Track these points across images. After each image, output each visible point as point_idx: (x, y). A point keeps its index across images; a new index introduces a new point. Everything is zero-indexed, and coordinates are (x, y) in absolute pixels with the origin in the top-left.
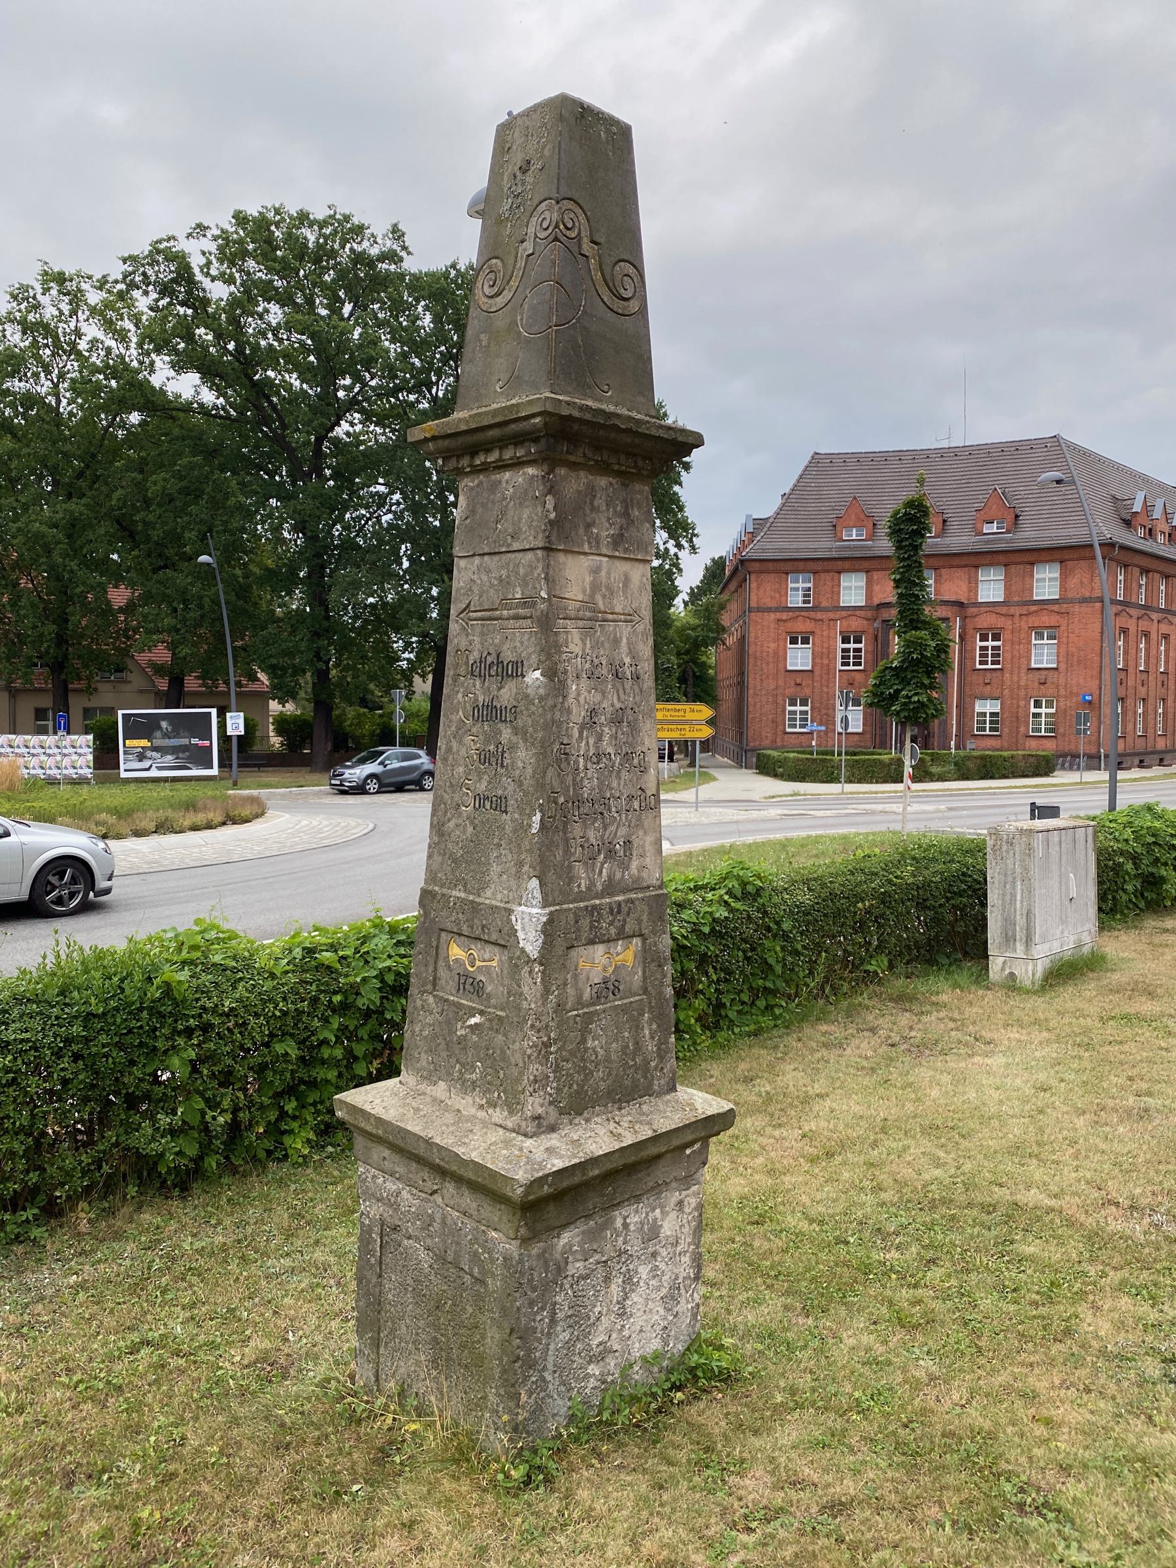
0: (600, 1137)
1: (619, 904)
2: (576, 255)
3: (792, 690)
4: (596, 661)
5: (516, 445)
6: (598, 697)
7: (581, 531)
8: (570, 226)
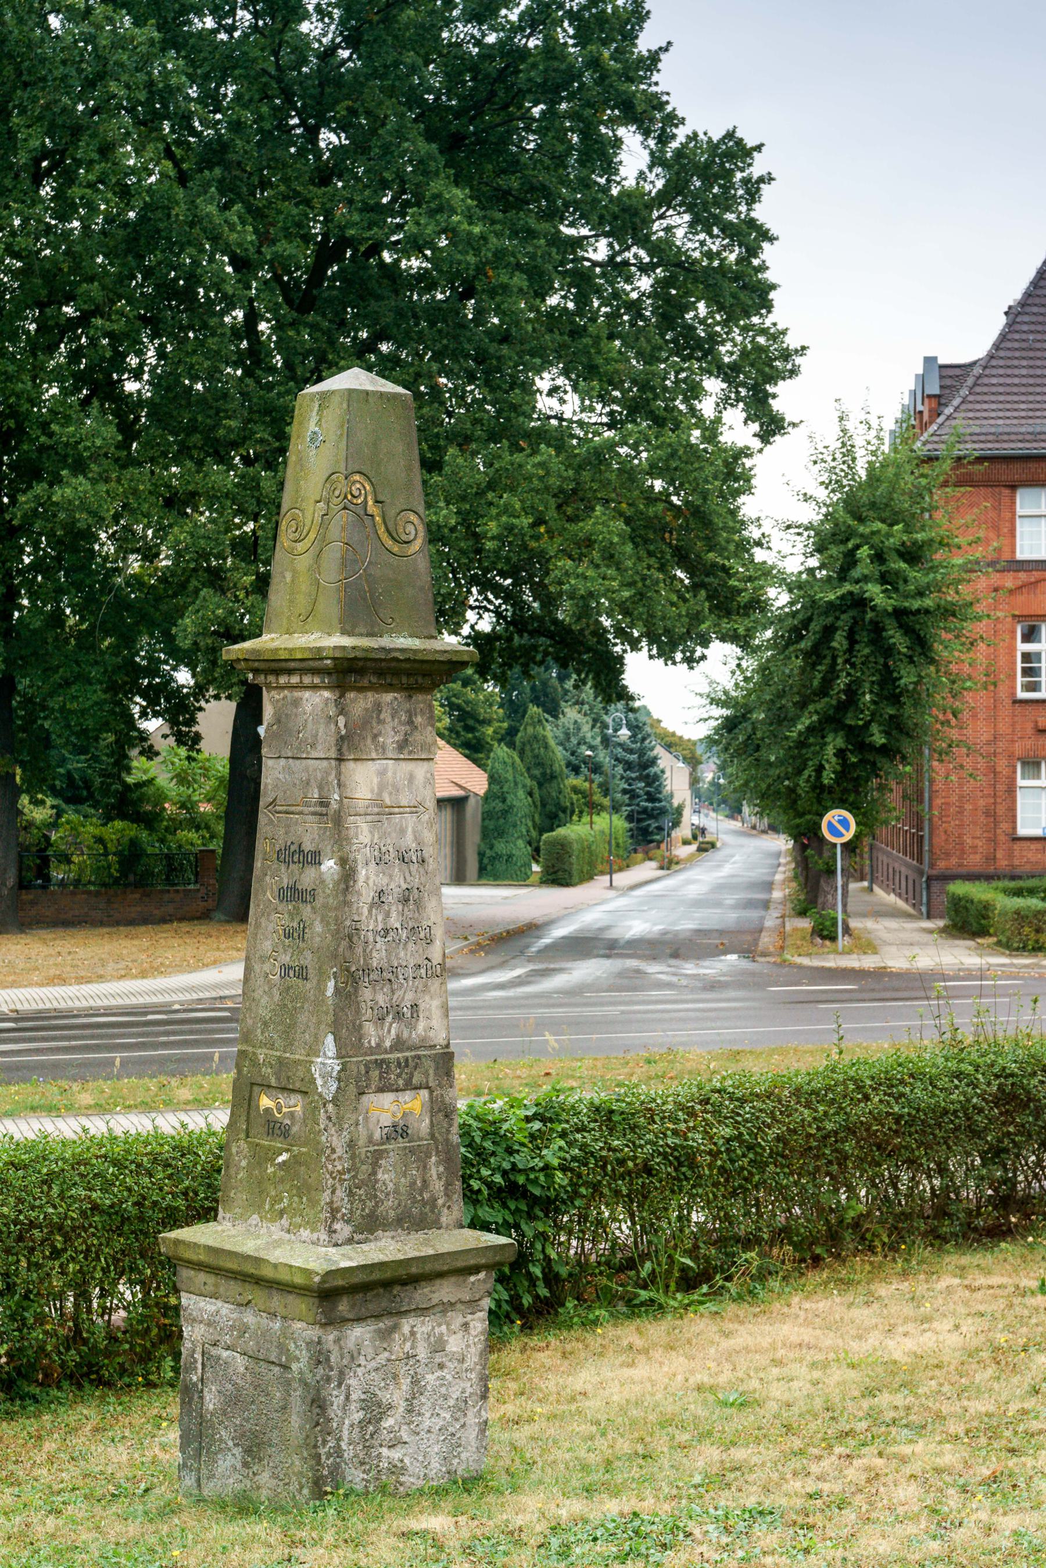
0: (386, 1249)
1: (407, 1060)
2: (363, 516)
3: (1029, 743)
6: (385, 880)
7: (369, 741)
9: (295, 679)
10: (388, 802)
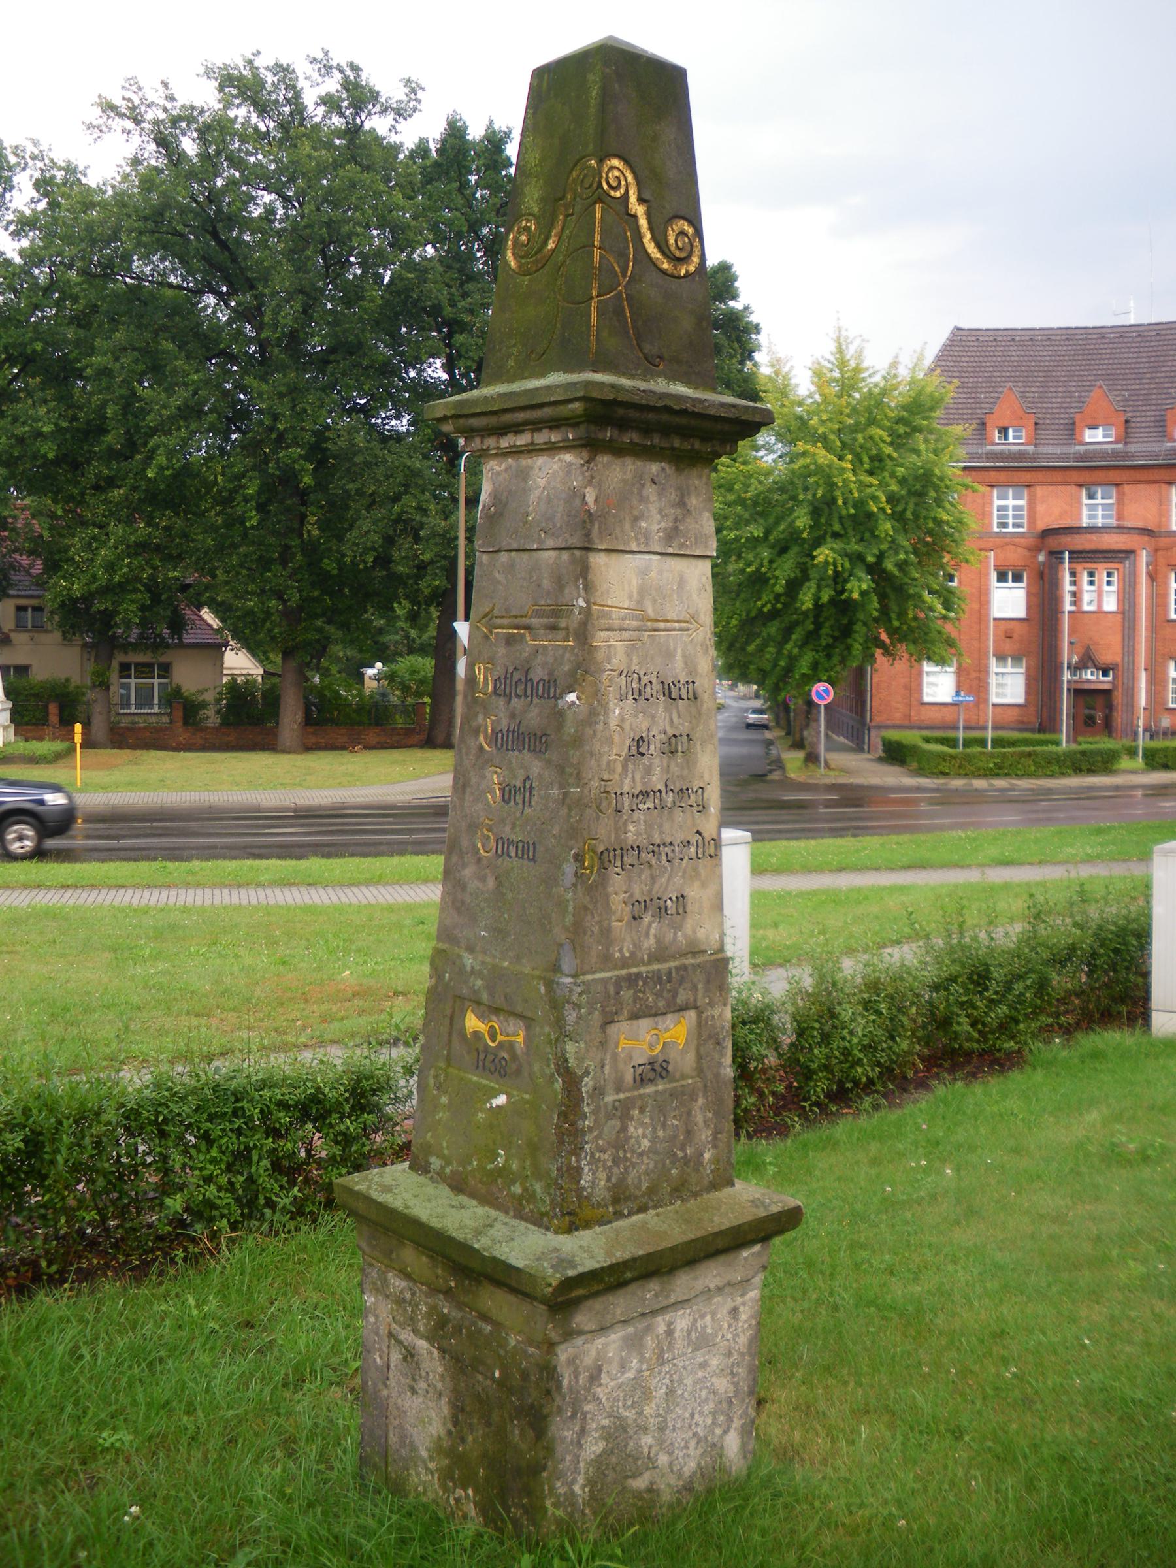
4: (645, 680)
5: (551, 428)
7: (627, 526)
8: (614, 184)
9: (522, 440)
10: (651, 613)
